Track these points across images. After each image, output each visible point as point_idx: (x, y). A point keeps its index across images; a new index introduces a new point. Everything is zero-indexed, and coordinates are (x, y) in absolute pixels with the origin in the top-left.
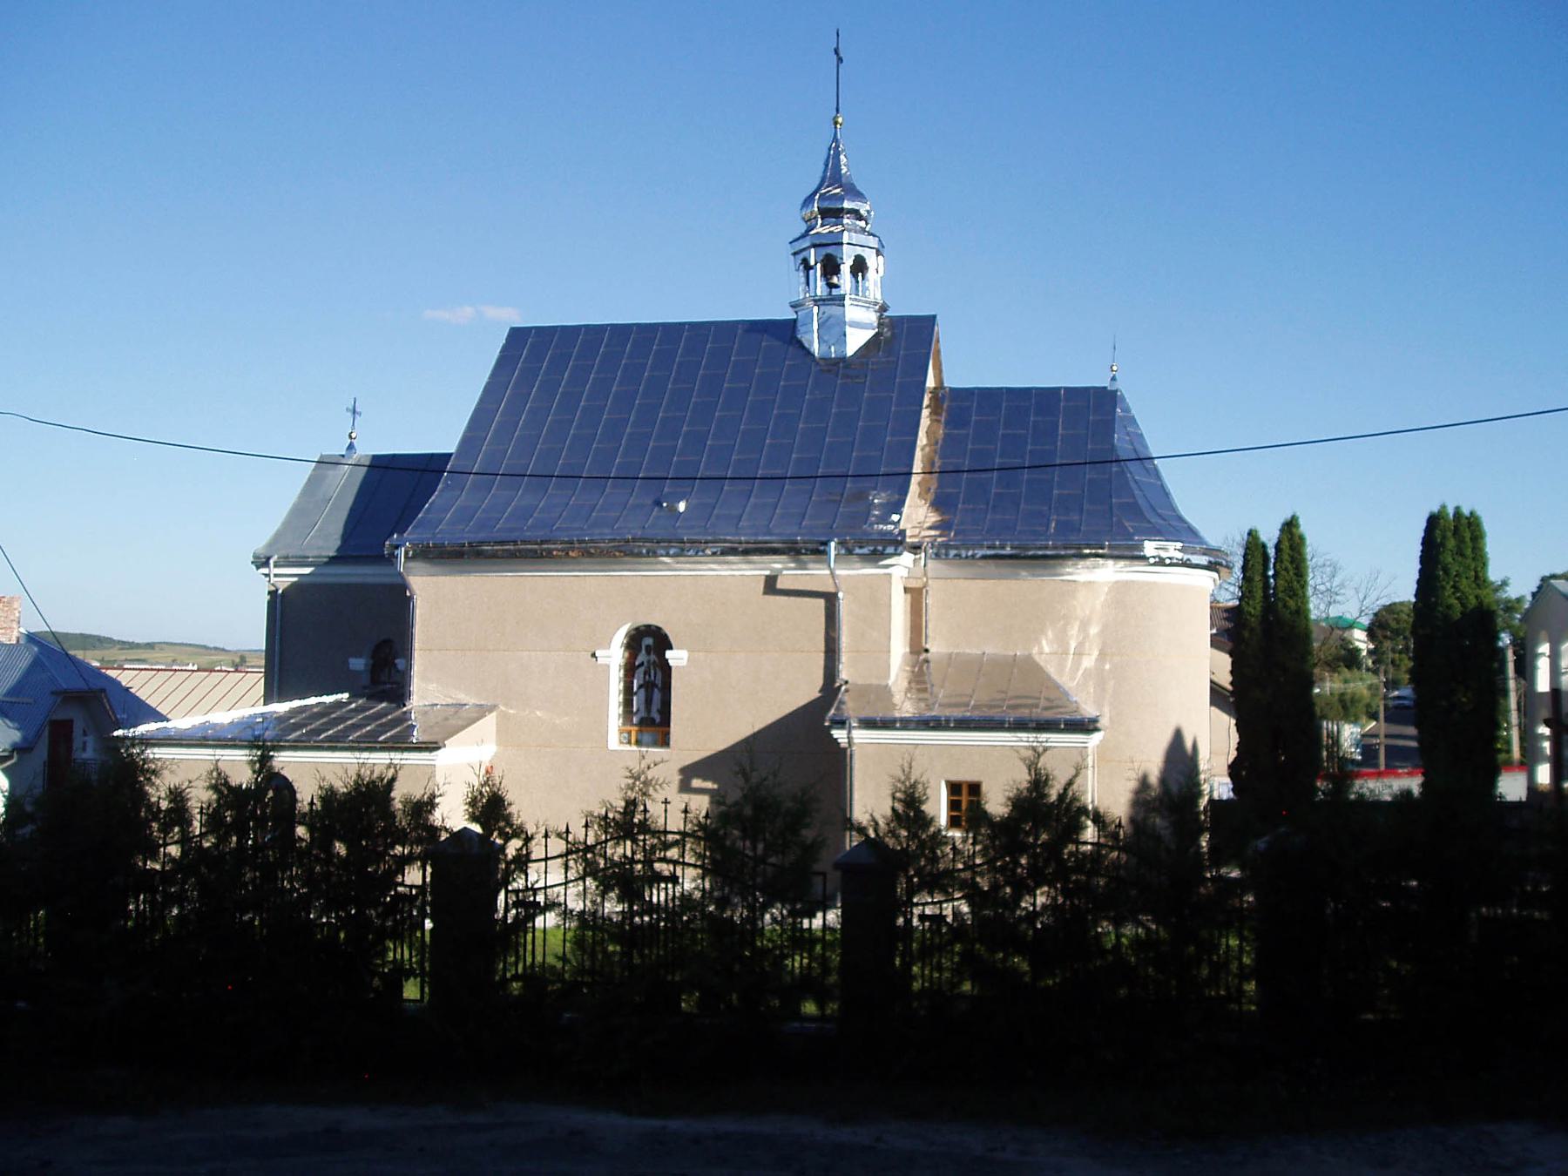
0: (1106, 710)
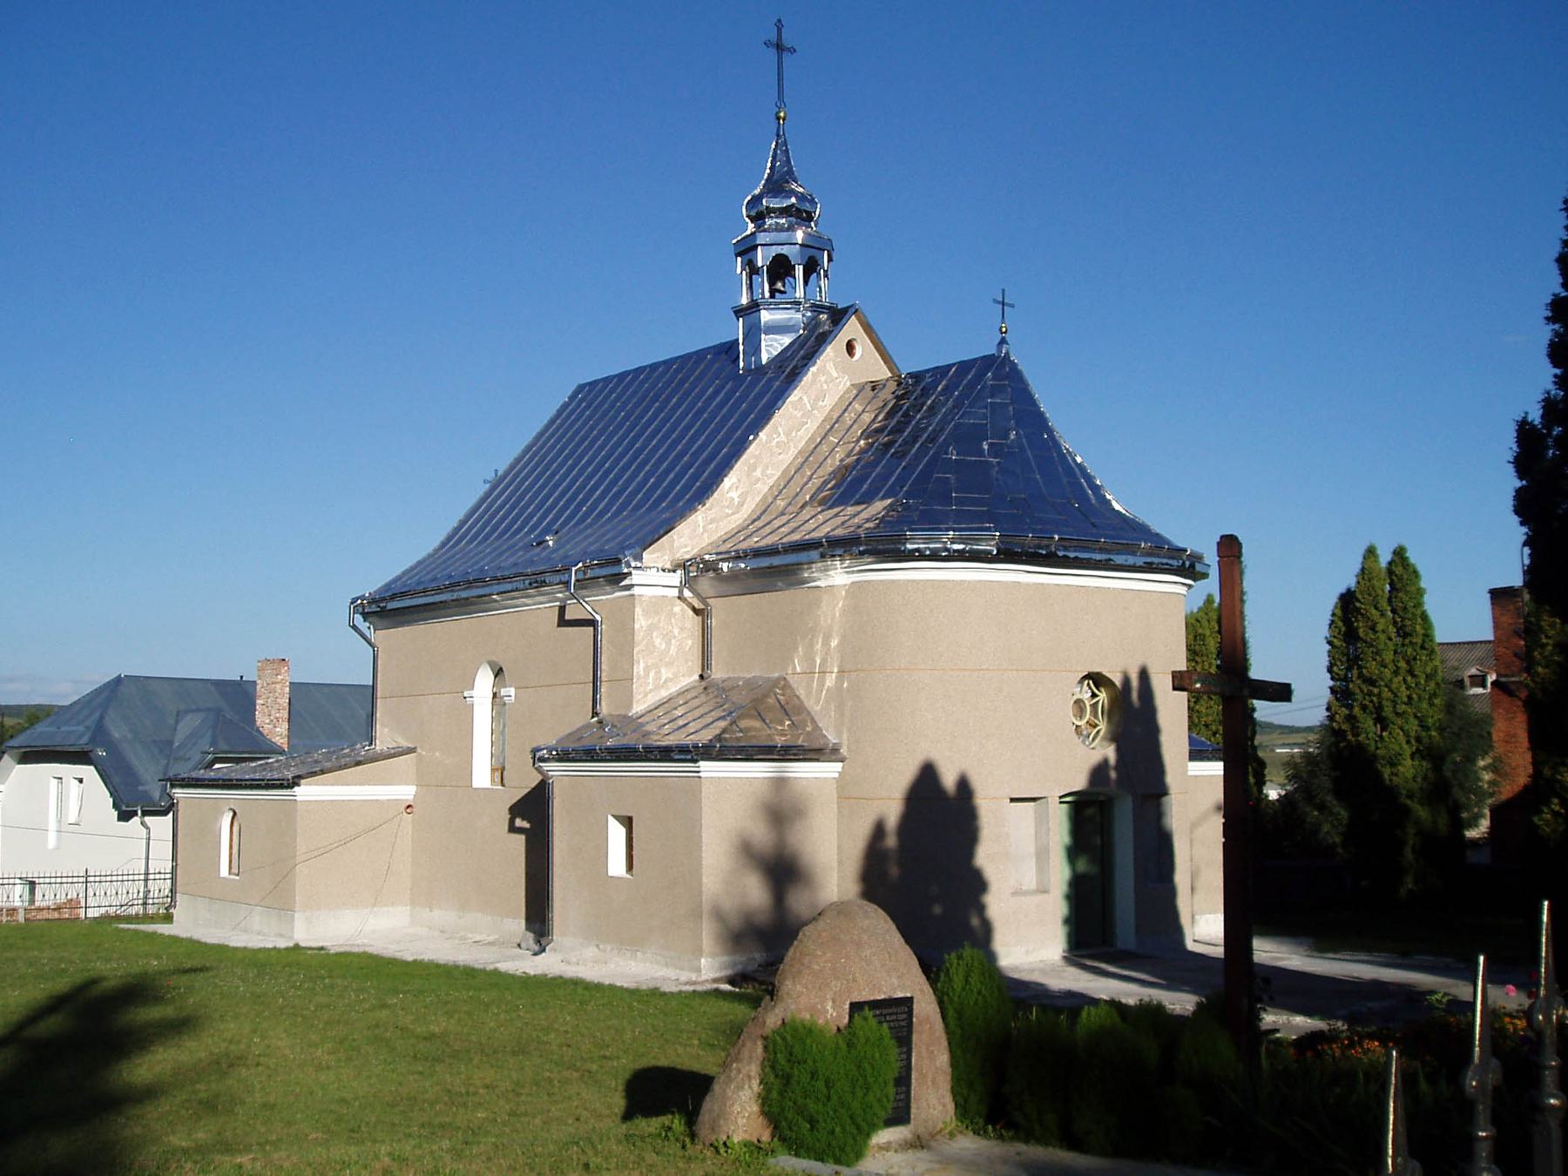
0: (845, 736)
